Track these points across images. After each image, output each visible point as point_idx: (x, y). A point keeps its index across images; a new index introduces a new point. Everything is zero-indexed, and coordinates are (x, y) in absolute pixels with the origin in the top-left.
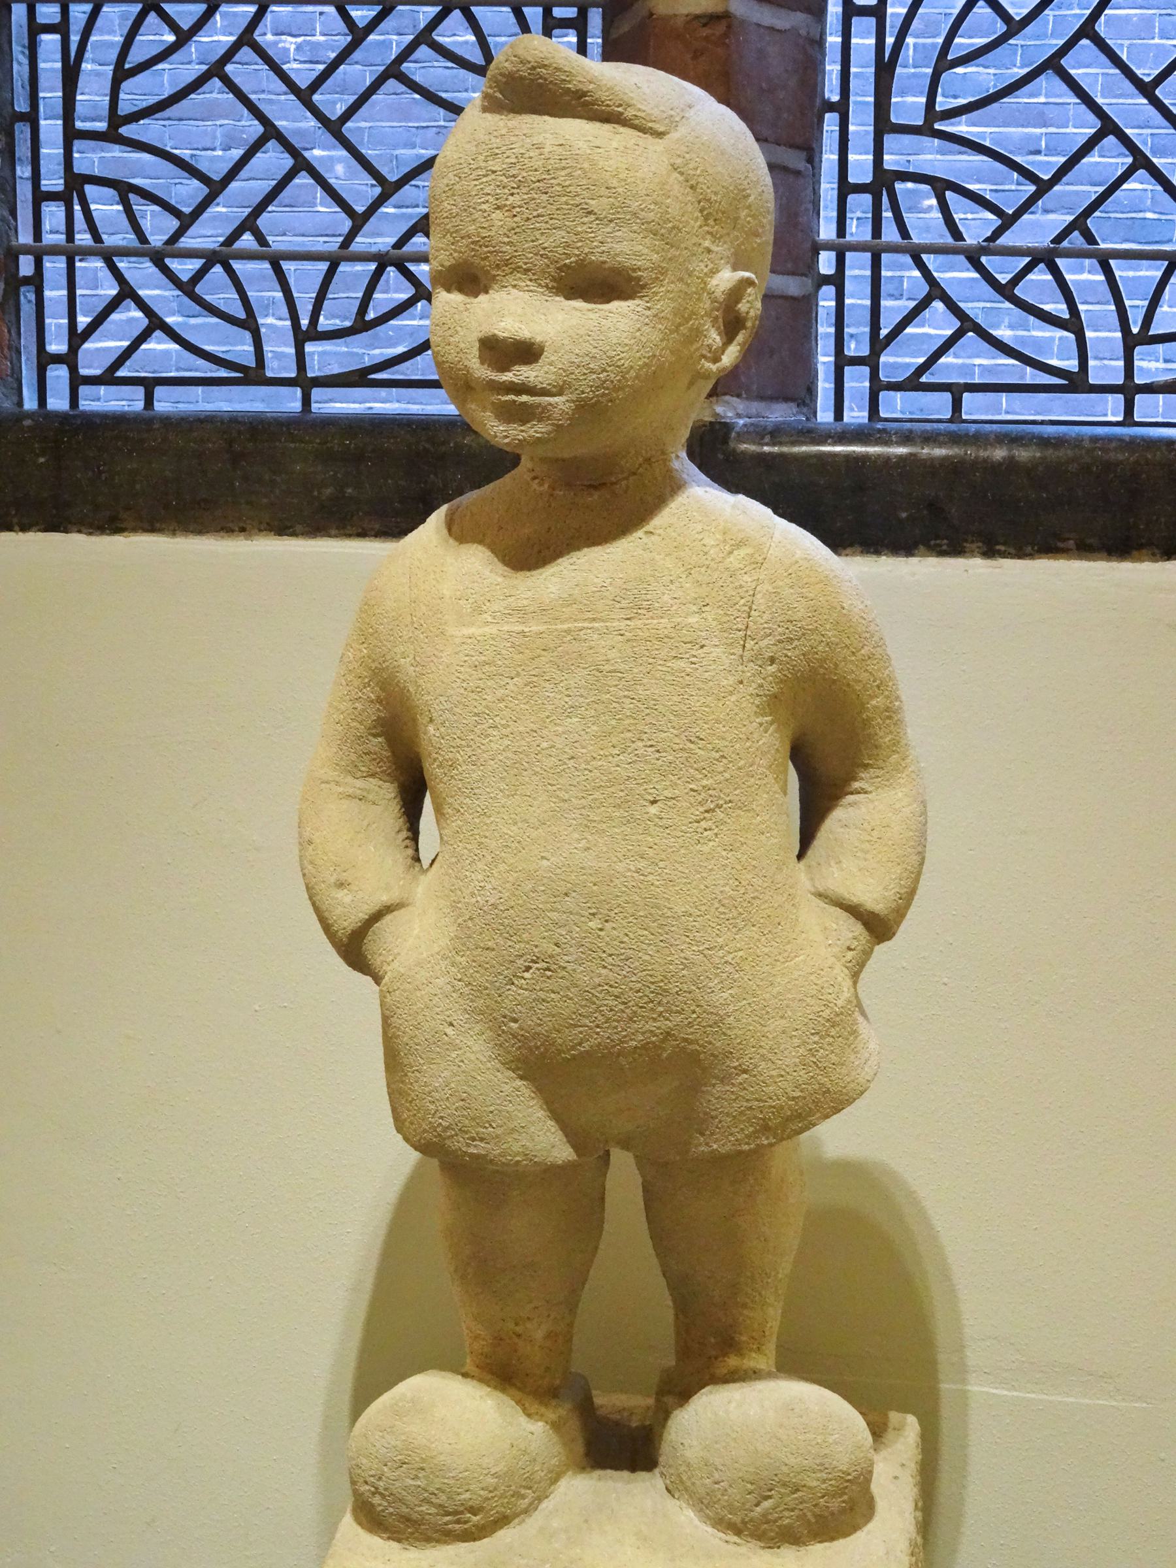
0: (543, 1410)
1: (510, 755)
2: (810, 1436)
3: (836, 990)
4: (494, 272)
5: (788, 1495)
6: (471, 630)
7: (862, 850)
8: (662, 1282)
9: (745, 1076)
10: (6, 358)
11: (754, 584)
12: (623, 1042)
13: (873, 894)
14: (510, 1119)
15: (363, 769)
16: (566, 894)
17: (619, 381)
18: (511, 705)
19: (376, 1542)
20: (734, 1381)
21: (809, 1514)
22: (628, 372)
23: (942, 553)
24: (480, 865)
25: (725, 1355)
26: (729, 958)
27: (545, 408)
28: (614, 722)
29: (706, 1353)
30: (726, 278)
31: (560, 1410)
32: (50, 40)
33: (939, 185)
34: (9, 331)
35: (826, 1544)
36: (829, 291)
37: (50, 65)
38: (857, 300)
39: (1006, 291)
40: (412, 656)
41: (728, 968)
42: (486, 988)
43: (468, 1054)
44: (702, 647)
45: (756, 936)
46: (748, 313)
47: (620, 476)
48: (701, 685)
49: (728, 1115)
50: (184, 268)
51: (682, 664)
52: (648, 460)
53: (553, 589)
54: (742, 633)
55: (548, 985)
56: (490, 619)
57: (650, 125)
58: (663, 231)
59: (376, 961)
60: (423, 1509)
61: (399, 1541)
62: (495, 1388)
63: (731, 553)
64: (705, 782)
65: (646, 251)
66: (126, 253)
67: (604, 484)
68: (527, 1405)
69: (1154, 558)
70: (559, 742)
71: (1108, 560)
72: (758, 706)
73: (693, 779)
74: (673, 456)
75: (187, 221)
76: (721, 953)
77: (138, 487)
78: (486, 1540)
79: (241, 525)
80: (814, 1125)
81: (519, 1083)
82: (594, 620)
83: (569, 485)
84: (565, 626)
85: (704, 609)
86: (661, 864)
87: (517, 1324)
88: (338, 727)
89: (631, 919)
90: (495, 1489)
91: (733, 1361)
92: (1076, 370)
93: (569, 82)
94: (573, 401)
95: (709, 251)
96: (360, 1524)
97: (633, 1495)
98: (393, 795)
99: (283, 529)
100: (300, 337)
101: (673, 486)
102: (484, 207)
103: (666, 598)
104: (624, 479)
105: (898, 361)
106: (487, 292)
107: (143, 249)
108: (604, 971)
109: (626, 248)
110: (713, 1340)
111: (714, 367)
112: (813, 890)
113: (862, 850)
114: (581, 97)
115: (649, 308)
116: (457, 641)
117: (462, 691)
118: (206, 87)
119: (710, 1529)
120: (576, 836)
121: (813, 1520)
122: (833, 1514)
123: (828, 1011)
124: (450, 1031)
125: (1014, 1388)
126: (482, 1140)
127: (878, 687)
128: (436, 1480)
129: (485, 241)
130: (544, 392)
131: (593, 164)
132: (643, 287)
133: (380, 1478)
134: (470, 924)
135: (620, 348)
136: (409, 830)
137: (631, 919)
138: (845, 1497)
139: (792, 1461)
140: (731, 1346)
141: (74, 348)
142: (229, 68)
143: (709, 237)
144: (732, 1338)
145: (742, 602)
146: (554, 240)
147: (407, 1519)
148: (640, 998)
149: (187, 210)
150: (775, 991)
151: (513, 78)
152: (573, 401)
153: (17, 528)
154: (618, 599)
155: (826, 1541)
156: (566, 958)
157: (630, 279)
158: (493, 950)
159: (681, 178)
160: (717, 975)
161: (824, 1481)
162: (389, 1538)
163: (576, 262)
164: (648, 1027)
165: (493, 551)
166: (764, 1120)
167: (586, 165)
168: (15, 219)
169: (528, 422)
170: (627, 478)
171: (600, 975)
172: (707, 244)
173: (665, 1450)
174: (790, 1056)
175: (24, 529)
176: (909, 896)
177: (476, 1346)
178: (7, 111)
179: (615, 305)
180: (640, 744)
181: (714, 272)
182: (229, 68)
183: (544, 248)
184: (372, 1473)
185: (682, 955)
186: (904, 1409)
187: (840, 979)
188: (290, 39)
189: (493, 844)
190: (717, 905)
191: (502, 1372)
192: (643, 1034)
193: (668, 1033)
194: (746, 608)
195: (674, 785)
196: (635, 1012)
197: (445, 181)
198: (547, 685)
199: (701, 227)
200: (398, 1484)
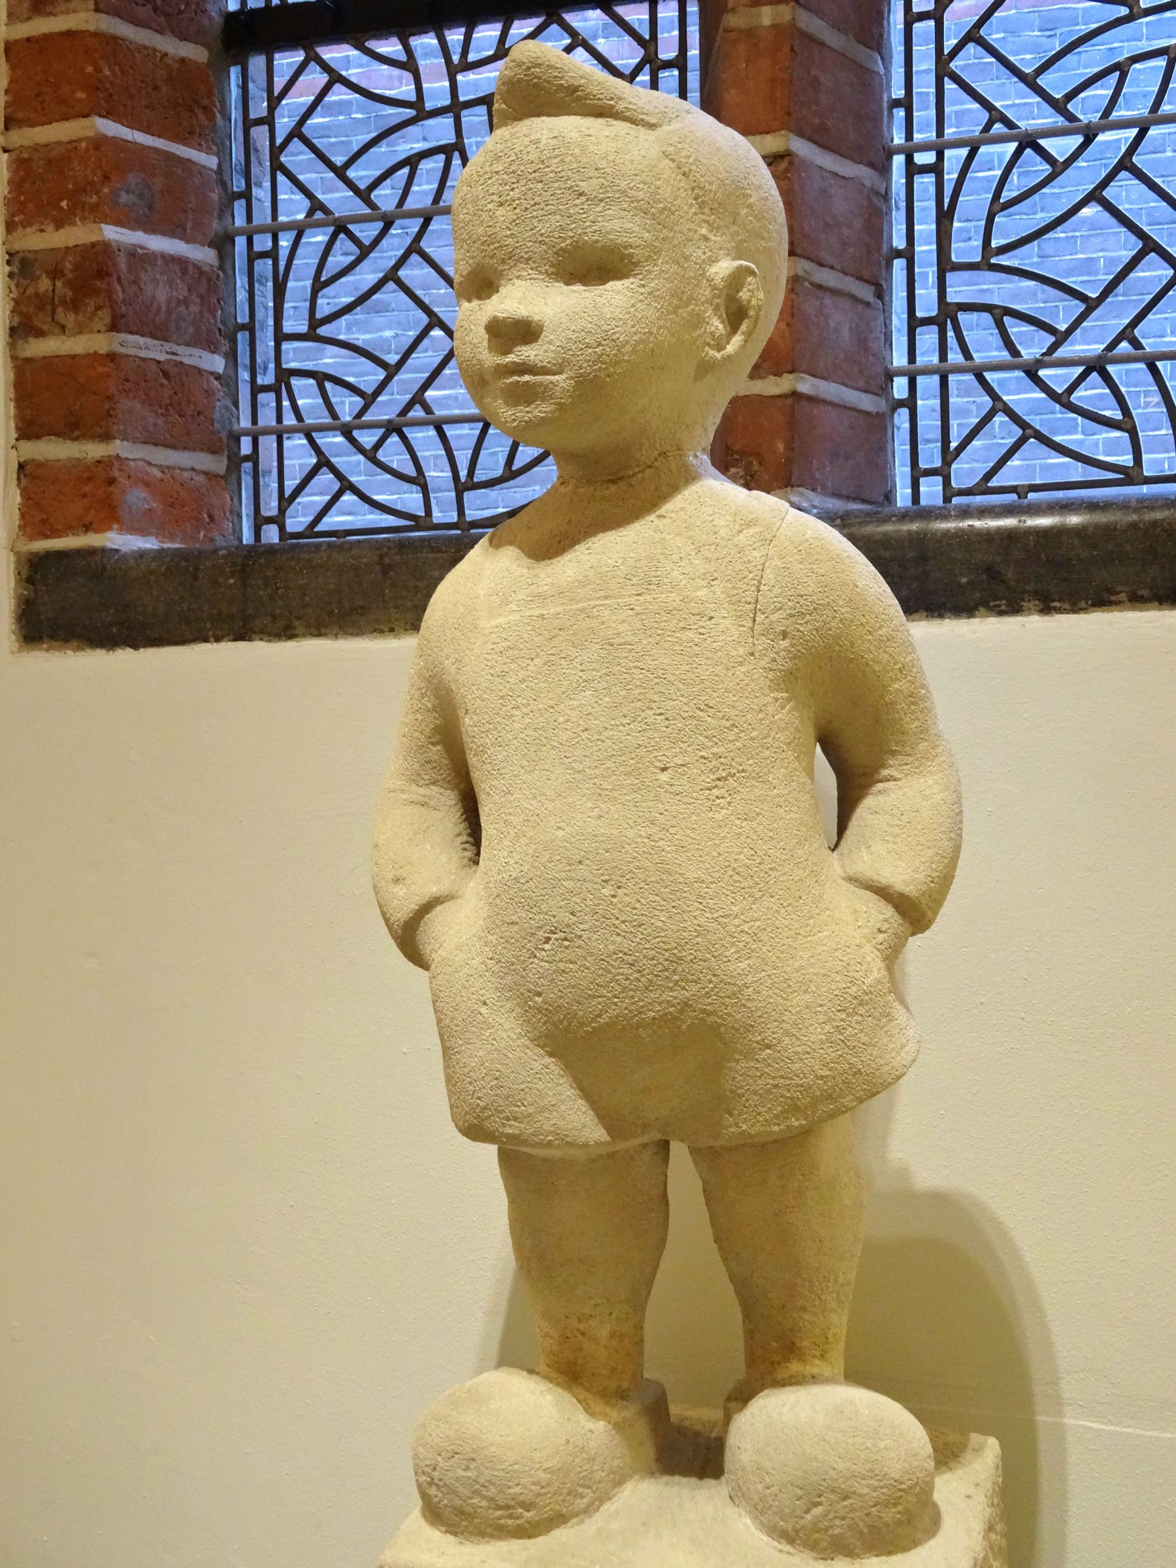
0: (608, 1410)
1: (531, 732)
3: (863, 968)
4: (501, 268)
5: (839, 1503)
6: (501, 620)
7: (891, 835)
8: (731, 1287)
9: (768, 1051)
12: (640, 1013)
13: (903, 876)
14: (541, 1096)
15: (426, 777)
16: (580, 862)
17: (615, 355)
18: (530, 684)
19: (435, 1535)
20: (791, 1384)
21: (861, 1524)
22: (624, 346)
23: (1001, 613)
25: (788, 1360)
26: (745, 927)
28: (624, 693)
29: (772, 1356)
30: (724, 267)
31: (626, 1411)
33: (997, 311)
34: (232, 499)
35: (884, 1558)
36: (904, 412)
38: (929, 423)
39: (1063, 400)
41: (745, 937)
42: (513, 964)
43: (500, 1032)
44: (711, 618)
45: (775, 908)
46: (749, 301)
47: (636, 470)
49: (755, 1093)
50: (367, 439)
51: (690, 634)
52: (664, 454)
53: (569, 573)
54: (752, 606)
56: (515, 608)
58: (653, 210)
59: (426, 950)
60: (475, 1501)
61: (455, 1535)
62: (558, 1384)
63: (740, 532)
64: (715, 750)
66: (322, 429)
68: (592, 1405)
71: (1160, 610)
72: (772, 681)
73: (703, 747)
74: (692, 453)
75: (369, 399)
76: (736, 922)
79: (391, 626)
81: (548, 1060)
82: (606, 597)
83: (589, 482)
84: (580, 606)
86: (672, 830)
87: (580, 1322)
88: (404, 740)
89: (642, 885)
90: (548, 1485)
91: (795, 1367)
92: (1131, 464)
93: (562, 78)
94: (572, 378)
95: (706, 239)
97: (698, 1501)
98: (454, 802)
100: (460, 488)
101: (689, 477)
102: (490, 206)
103: (675, 573)
104: (640, 472)
105: (966, 471)
108: (619, 939)
109: (618, 226)
110: (775, 1344)
111: (719, 355)
112: (843, 875)
115: (643, 286)
116: (486, 632)
117: (489, 677)
118: (384, 289)
119: (765, 1538)
120: (590, 805)
121: (866, 1530)
122: (887, 1525)
123: (855, 988)
124: (483, 1010)
125: (1111, 1423)
126: (515, 1119)
127: (900, 670)
128: (486, 1472)
129: (492, 239)
130: (545, 371)
131: (583, 149)
132: (636, 264)
133: (435, 1469)
134: (498, 901)
135: (614, 323)
136: (469, 835)
137: (642, 885)
138: (900, 1508)
139: (841, 1465)
141: (282, 511)
142: (402, 273)
143: (704, 225)
144: (794, 1343)
145: (751, 576)
146: (549, 225)
147: (461, 1512)
148: (655, 965)
150: (797, 965)
151: (513, 84)
152: (572, 378)
153: (212, 639)
155: (882, 1555)
156: (581, 926)
157: (622, 257)
158: (517, 924)
159: (673, 165)
160: (733, 944)
161: (875, 1489)
162: (446, 1532)
163: (571, 244)
164: (664, 998)
166: (791, 1099)
167: (577, 151)
168: (237, 408)
171: (614, 943)
172: (704, 231)
174: (816, 1034)
175: (218, 640)
180: (651, 713)
181: (713, 260)
182: (402, 273)
183: (541, 235)
184: (428, 1462)
185: (695, 922)
186: (986, 1432)
187: (868, 959)
190: (731, 873)
191: (570, 1372)
192: (660, 1003)
193: (686, 1004)
196: (650, 981)
198: (563, 662)
199: (696, 214)
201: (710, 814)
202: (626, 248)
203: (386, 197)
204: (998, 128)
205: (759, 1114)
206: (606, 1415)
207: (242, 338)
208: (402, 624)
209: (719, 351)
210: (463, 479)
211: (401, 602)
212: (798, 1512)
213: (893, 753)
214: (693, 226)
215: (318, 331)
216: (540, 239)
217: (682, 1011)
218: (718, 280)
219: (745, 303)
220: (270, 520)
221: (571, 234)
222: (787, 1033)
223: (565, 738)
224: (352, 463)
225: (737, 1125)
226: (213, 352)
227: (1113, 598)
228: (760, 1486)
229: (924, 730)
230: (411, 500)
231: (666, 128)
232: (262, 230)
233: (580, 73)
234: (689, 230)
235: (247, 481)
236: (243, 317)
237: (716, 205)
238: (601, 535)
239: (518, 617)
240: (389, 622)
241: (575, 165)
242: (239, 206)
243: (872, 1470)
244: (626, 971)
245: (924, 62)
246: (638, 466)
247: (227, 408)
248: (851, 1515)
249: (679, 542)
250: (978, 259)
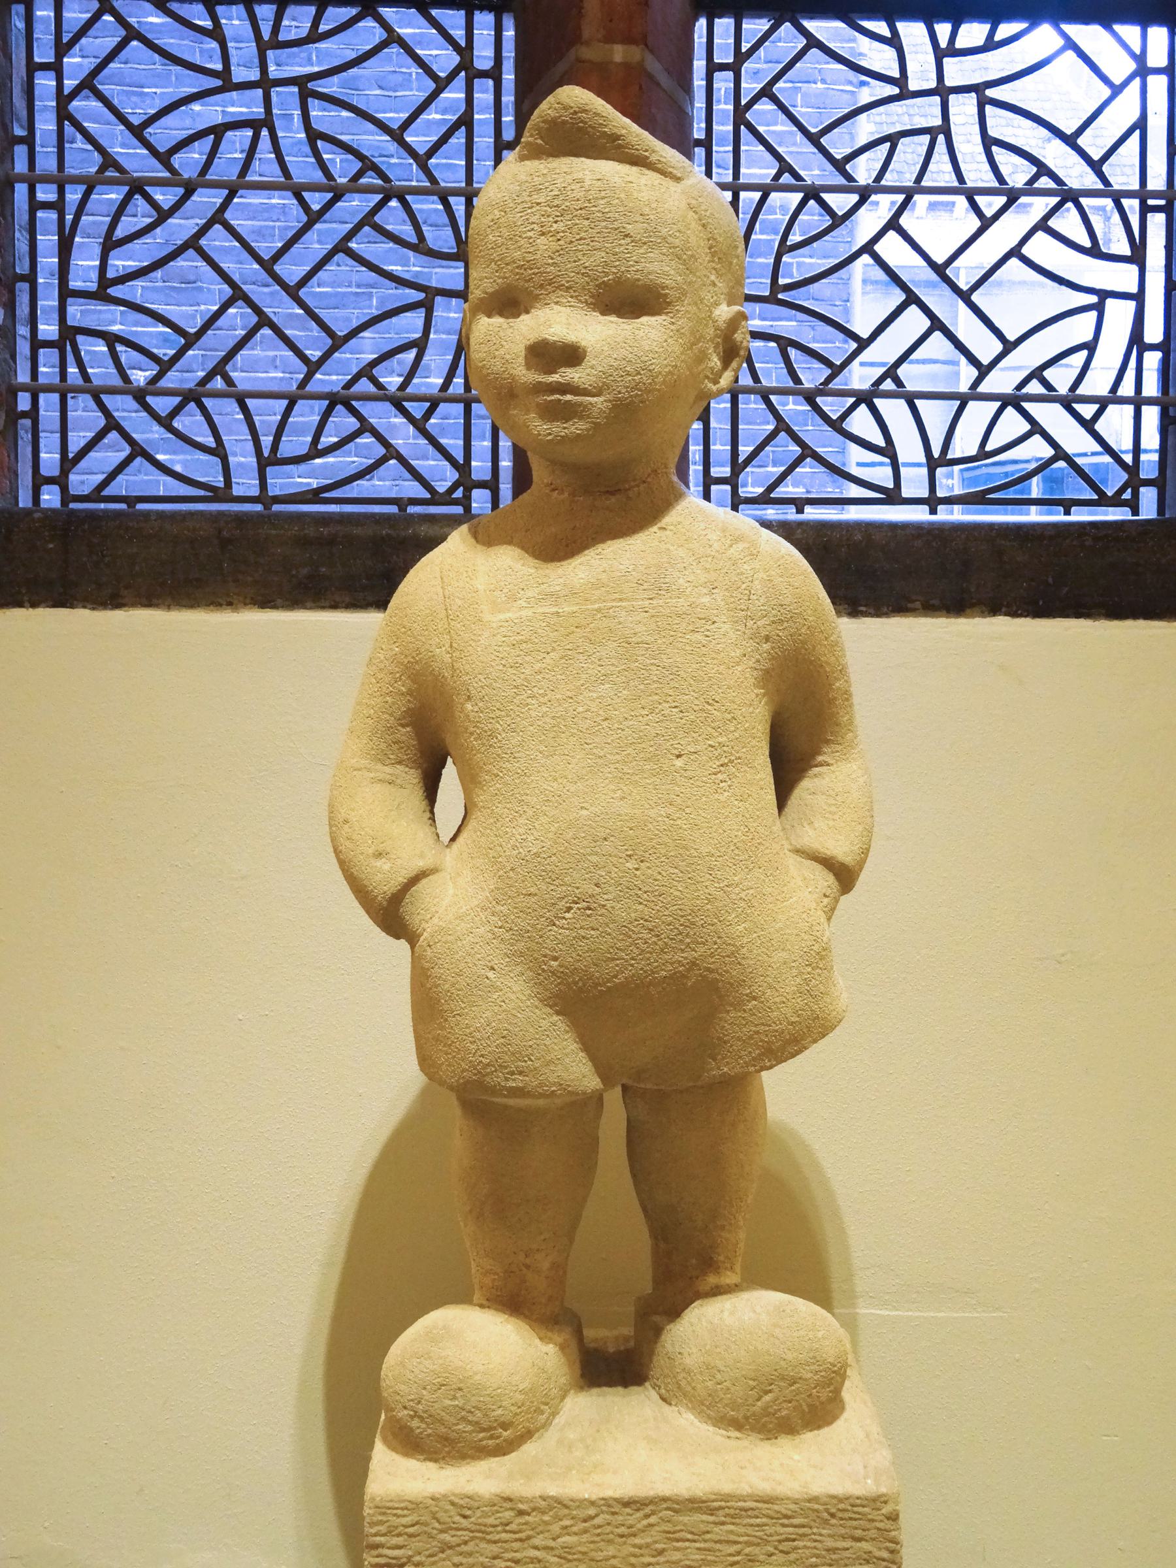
0: (549, 1334)
1: (548, 720)
2: (802, 1333)
6: (508, 615)
7: (830, 813)
9: (754, 1002)
10: (5, 477)
13: (841, 849)
16: (605, 839)
20: (721, 1294)
24: (522, 821)
25: (705, 1274)
26: (743, 895)
28: (642, 687)
32: (47, 217)
37: (48, 240)
40: (447, 645)
48: (714, 655)
49: (739, 1039)
50: (163, 404)
51: (699, 637)
52: (655, 471)
55: (592, 922)
56: (524, 604)
60: (460, 1427)
61: (436, 1461)
62: (511, 1315)
64: (720, 739)
65: (672, 272)
69: (983, 615)
70: (594, 706)
73: (710, 737)
75: (165, 366)
76: (737, 890)
77: (137, 568)
78: (513, 1454)
80: (806, 1048)
81: (555, 1018)
82: (621, 600)
84: (596, 606)
86: (688, 810)
91: (712, 1280)
94: (610, 401)
95: (714, 285)
96: (394, 1449)
97: (634, 1407)
99: (265, 602)
100: (263, 462)
103: (681, 581)
106: (527, 312)
107: (126, 387)
109: (657, 267)
113: (830, 813)
114: (614, 141)
117: (501, 667)
119: (711, 1428)
124: (491, 974)
126: (520, 1073)
128: (473, 1399)
129: (531, 265)
132: (669, 304)
139: (790, 1356)
140: (710, 1266)
142: (203, 242)
144: (711, 1258)
145: (744, 586)
147: (446, 1439)
153: (27, 604)
156: (606, 897)
157: (659, 295)
159: (696, 217)
163: (613, 280)
165: (523, 548)
167: (622, 196)
168: (15, 363)
169: (570, 420)
170: (638, 486)
172: (713, 278)
173: (659, 1363)
174: (790, 984)
175: (34, 605)
176: (866, 852)
177: (487, 1281)
178: (10, 273)
180: (667, 705)
188: (140, 373)
189: (533, 800)
191: (511, 1301)
195: (696, 742)
197: (490, 217)
200: (436, 1406)
201: (716, 796)
202: (663, 288)
203: (190, 160)
204: (786, 178)
205: (740, 1057)
206: (550, 1339)
207: (23, 288)
208: (241, 599)
210: (266, 454)
211: (240, 577)
212: (750, 1401)
213: (828, 742)
215: (109, 291)
216: (583, 271)
217: (688, 970)
220: (50, 481)
221: (614, 270)
222: (770, 987)
223: (586, 726)
224: (149, 433)
225: (719, 1068)
227: (909, 605)
228: (709, 1384)
229: (851, 722)
230: (209, 471)
232: (46, 179)
235: (25, 437)
236: (22, 268)
237: (721, 256)
238: (609, 542)
239: (530, 614)
240: (228, 595)
241: (621, 209)
242: (21, 151)
243: (815, 1357)
244: (646, 936)
245: (724, 107)
246: (635, 480)
248: (797, 1398)
249: (681, 552)
250: (767, 294)
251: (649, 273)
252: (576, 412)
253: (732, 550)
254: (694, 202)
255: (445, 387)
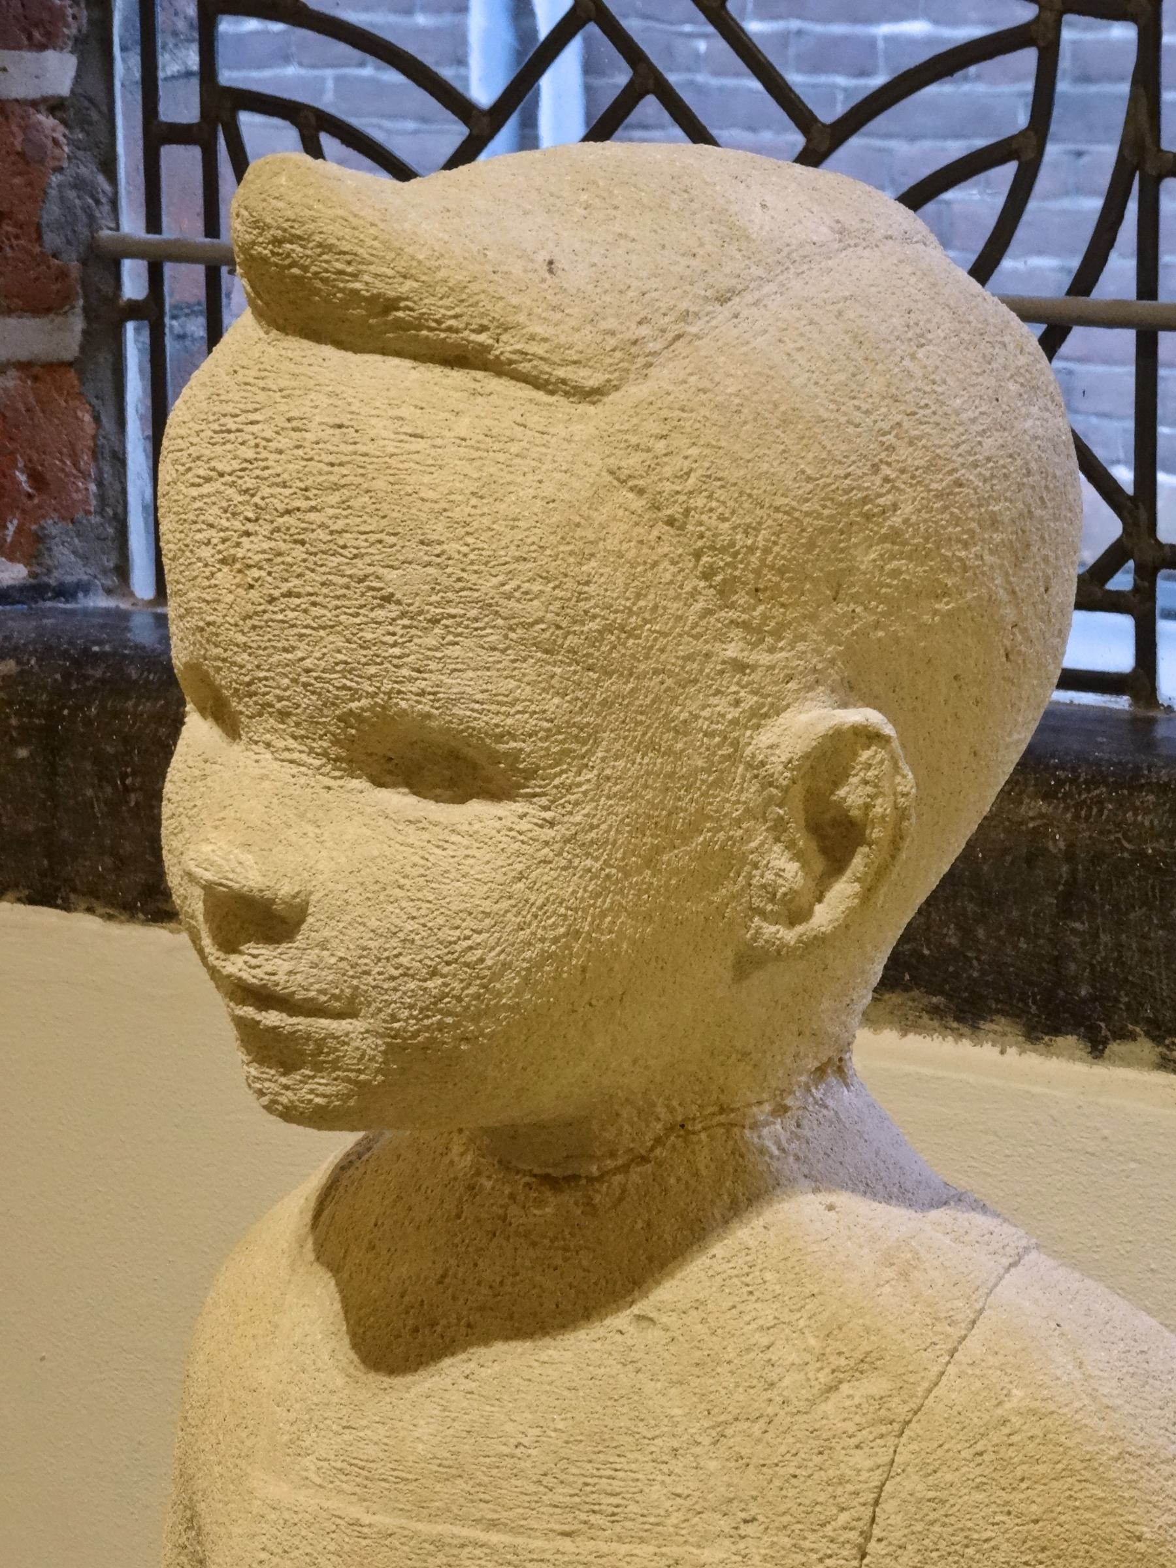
10: (85, 476)
11: (876, 1478)
17: (477, 997)
22: (497, 976)
27: (320, 1043)
30: (811, 718)
34: (97, 419)
46: (867, 807)
47: (610, 1163)
57: (561, 373)
58: (572, 641)
63: (831, 1389)
67: (576, 1178)
82: (493, 1525)
85: (746, 1529)
93: (355, 276)
103: (656, 1492)
104: (617, 1170)
109: (469, 685)
111: (790, 936)
115: (552, 824)
132: (531, 774)
135: (471, 923)
145: (844, 1518)
149: (621, 77)
152: (378, 1035)
154: (549, 1481)
157: (495, 757)
159: (638, 504)
163: (371, 708)
167: (380, 484)
172: (732, 651)
179: (477, 807)
183: (308, 671)
194: (853, 1536)
199: (708, 612)
202: (499, 738)
209: (792, 922)
214: (701, 646)
218: (776, 765)
219: (855, 813)
221: (367, 686)
226: (42, 47)
231: (635, 391)
233: (401, 265)
234: (690, 658)
238: (499, 1347)
246: (613, 1155)
247: (80, 184)
251: (454, 702)
252: (302, 1053)
253: (828, 1407)
254: (634, 461)
255: (1086, 277)
